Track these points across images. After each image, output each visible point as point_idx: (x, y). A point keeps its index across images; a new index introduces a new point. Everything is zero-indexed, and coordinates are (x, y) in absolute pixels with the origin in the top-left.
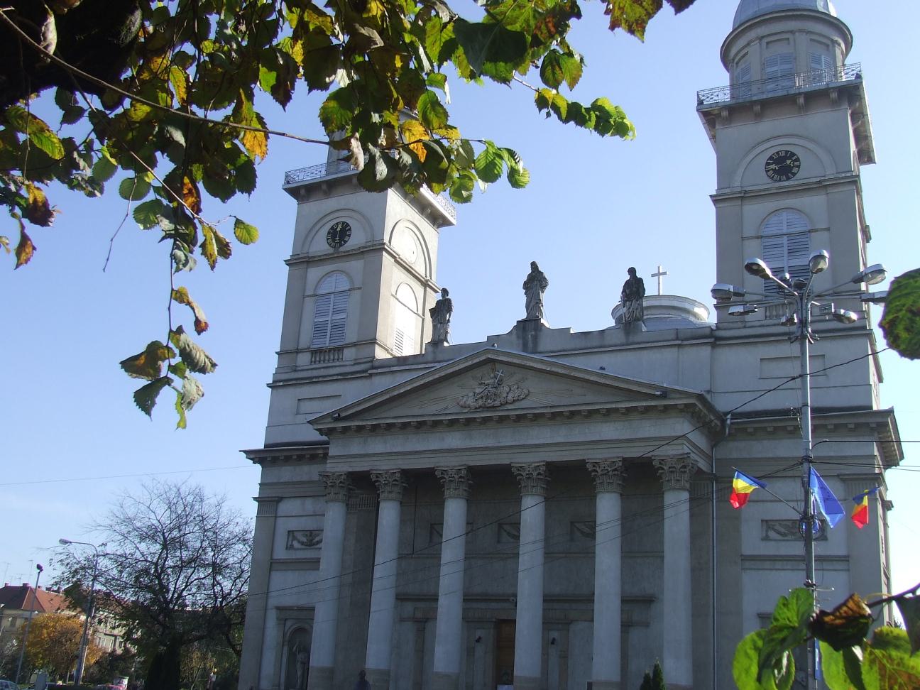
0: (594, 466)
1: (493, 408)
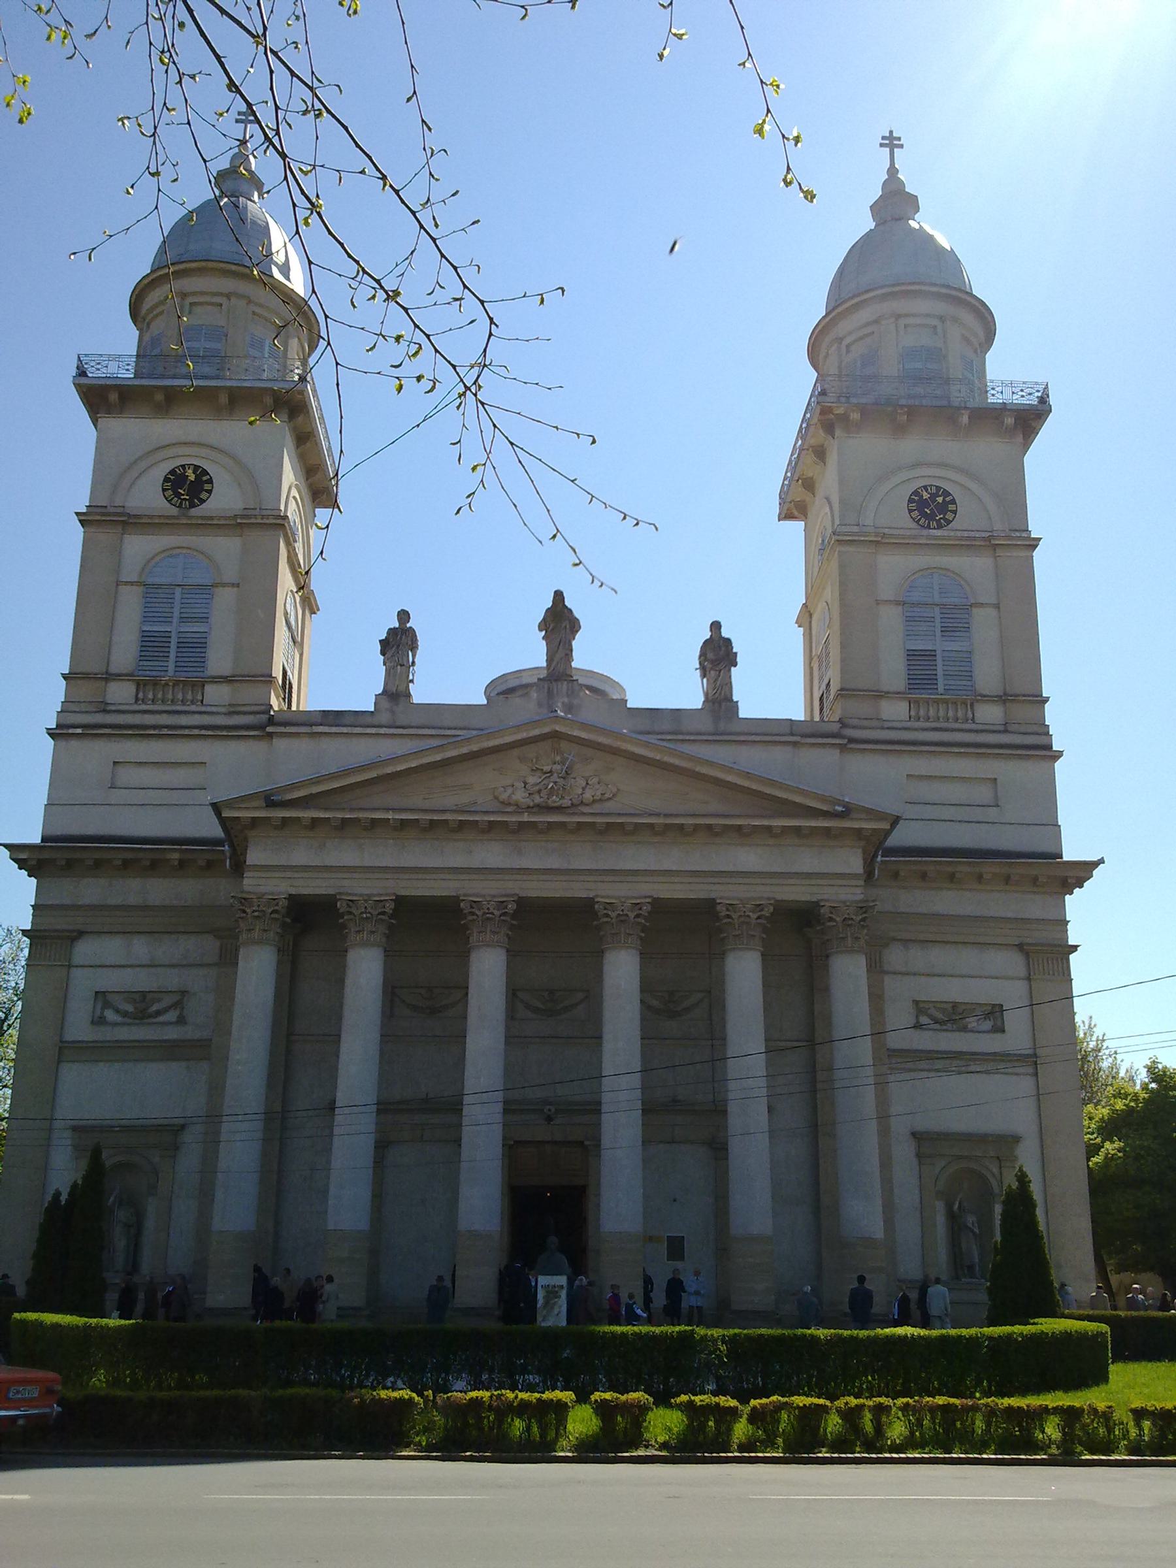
0: (728, 910)
1: (559, 809)
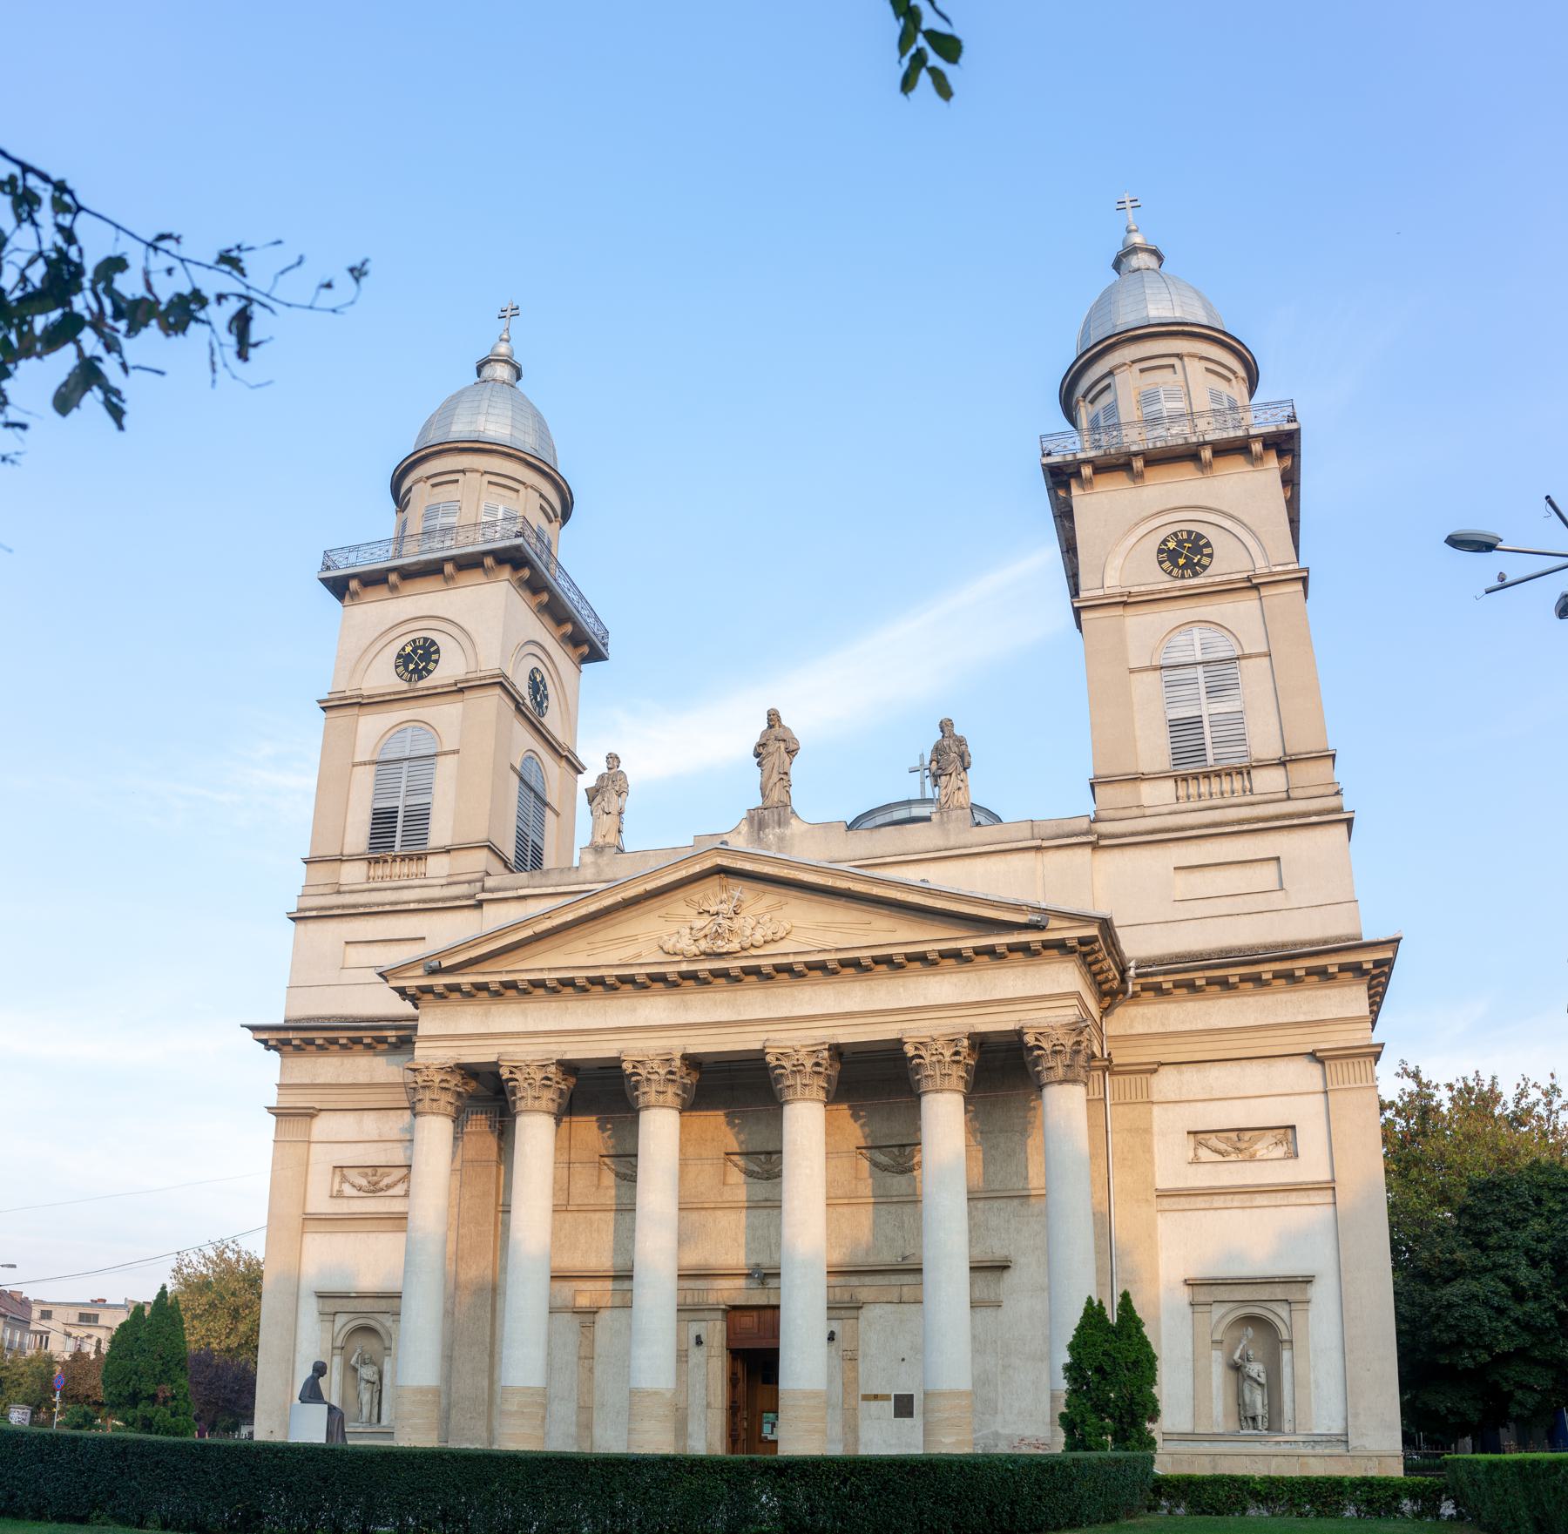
0: (778, 1059)
